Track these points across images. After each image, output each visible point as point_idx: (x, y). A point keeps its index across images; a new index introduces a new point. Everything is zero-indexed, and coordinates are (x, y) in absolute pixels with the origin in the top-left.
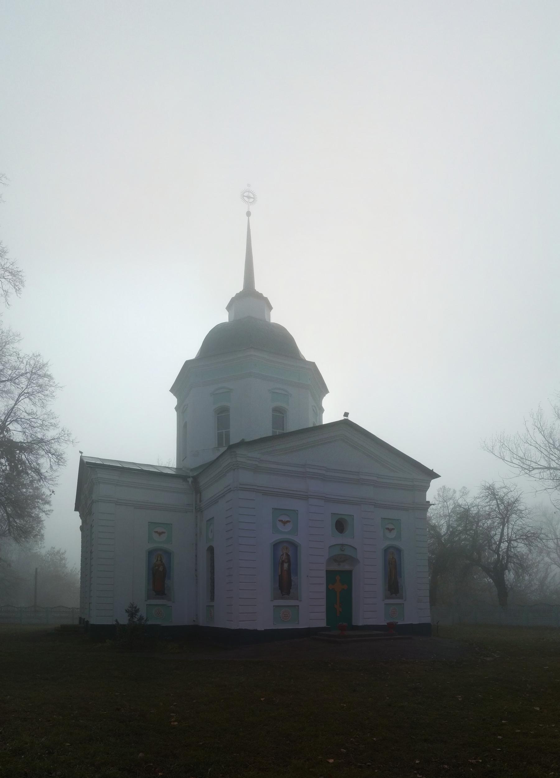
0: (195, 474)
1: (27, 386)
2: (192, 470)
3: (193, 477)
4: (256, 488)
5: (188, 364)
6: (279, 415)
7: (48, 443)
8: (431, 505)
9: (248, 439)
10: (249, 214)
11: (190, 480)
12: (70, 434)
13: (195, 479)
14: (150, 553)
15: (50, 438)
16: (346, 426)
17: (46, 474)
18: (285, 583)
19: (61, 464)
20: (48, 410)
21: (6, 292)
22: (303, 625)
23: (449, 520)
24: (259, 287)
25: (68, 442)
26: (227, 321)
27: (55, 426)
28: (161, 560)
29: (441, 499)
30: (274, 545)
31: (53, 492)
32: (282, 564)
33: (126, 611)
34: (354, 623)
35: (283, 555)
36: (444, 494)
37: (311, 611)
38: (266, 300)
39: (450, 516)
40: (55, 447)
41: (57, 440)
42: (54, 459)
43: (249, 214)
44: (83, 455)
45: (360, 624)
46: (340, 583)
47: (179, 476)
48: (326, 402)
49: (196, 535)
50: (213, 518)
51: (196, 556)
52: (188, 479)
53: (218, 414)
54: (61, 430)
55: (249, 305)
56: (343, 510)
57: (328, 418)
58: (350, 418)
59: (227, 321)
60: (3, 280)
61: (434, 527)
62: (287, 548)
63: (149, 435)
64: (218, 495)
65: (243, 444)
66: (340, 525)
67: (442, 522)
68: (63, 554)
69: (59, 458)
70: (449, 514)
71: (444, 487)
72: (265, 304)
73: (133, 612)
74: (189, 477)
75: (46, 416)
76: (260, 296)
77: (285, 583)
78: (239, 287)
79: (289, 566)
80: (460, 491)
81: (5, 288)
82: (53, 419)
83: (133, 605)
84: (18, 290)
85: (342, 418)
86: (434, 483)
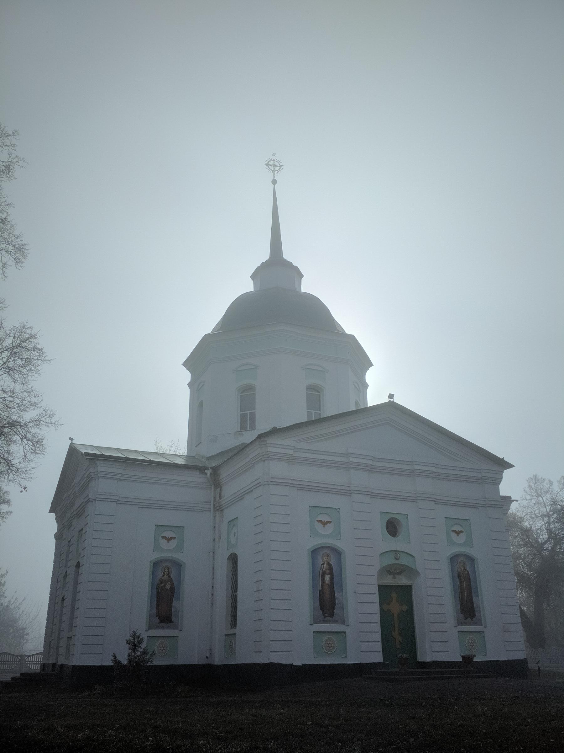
0: (214, 465)
1: (8, 359)
2: (209, 458)
3: (212, 468)
4: (290, 481)
5: (206, 336)
6: (314, 394)
7: (25, 425)
8: (513, 501)
10: (274, 182)
11: (209, 472)
12: (54, 414)
13: (215, 470)
14: (155, 564)
16: (391, 407)
17: (19, 466)
18: (327, 604)
19: (39, 452)
20: (30, 386)
21: (4, 264)
22: (351, 660)
23: (549, 523)
24: (288, 255)
25: (50, 425)
26: (252, 289)
28: (168, 575)
29: (533, 493)
30: (312, 552)
32: (323, 576)
33: (127, 641)
34: (420, 659)
35: (323, 564)
36: (536, 485)
37: (362, 642)
38: (296, 268)
39: (548, 516)
40: (33, 432)
41: (37, 422)
43: (274, 182)
44: (74, 442)
45: (428, 660)
46: (397, 602)
47: (191, 466)
48: (371, 376)
49: (214, 540)
50: (237, 518)
51: (213, 568)
52: (206, 471)
53: (242, 393)
54: (42, 410)
55: (277, 273)
56: (395, 508)
57: (374, 397)
58: (396, 400)
59: (252, 289)
60: (3, 253)
61: (527, 532)
63: (158, 419)
66: (392, 527)
67: (539, 524)
69: (37, 445)
70: (548, 513)
71: (535, 476)
72: (296, 274)
73: (134, 643)
74: (207, 468)
75: (25, 394)
76: (289, 265)
77: (327, 604)
78: (264, 255)
80: (559, 482)
81: (4, 260)
82: (35, 397)
83: (135, 634)
84: (18, 261)
85: (387, 400)
86: (507, 473)
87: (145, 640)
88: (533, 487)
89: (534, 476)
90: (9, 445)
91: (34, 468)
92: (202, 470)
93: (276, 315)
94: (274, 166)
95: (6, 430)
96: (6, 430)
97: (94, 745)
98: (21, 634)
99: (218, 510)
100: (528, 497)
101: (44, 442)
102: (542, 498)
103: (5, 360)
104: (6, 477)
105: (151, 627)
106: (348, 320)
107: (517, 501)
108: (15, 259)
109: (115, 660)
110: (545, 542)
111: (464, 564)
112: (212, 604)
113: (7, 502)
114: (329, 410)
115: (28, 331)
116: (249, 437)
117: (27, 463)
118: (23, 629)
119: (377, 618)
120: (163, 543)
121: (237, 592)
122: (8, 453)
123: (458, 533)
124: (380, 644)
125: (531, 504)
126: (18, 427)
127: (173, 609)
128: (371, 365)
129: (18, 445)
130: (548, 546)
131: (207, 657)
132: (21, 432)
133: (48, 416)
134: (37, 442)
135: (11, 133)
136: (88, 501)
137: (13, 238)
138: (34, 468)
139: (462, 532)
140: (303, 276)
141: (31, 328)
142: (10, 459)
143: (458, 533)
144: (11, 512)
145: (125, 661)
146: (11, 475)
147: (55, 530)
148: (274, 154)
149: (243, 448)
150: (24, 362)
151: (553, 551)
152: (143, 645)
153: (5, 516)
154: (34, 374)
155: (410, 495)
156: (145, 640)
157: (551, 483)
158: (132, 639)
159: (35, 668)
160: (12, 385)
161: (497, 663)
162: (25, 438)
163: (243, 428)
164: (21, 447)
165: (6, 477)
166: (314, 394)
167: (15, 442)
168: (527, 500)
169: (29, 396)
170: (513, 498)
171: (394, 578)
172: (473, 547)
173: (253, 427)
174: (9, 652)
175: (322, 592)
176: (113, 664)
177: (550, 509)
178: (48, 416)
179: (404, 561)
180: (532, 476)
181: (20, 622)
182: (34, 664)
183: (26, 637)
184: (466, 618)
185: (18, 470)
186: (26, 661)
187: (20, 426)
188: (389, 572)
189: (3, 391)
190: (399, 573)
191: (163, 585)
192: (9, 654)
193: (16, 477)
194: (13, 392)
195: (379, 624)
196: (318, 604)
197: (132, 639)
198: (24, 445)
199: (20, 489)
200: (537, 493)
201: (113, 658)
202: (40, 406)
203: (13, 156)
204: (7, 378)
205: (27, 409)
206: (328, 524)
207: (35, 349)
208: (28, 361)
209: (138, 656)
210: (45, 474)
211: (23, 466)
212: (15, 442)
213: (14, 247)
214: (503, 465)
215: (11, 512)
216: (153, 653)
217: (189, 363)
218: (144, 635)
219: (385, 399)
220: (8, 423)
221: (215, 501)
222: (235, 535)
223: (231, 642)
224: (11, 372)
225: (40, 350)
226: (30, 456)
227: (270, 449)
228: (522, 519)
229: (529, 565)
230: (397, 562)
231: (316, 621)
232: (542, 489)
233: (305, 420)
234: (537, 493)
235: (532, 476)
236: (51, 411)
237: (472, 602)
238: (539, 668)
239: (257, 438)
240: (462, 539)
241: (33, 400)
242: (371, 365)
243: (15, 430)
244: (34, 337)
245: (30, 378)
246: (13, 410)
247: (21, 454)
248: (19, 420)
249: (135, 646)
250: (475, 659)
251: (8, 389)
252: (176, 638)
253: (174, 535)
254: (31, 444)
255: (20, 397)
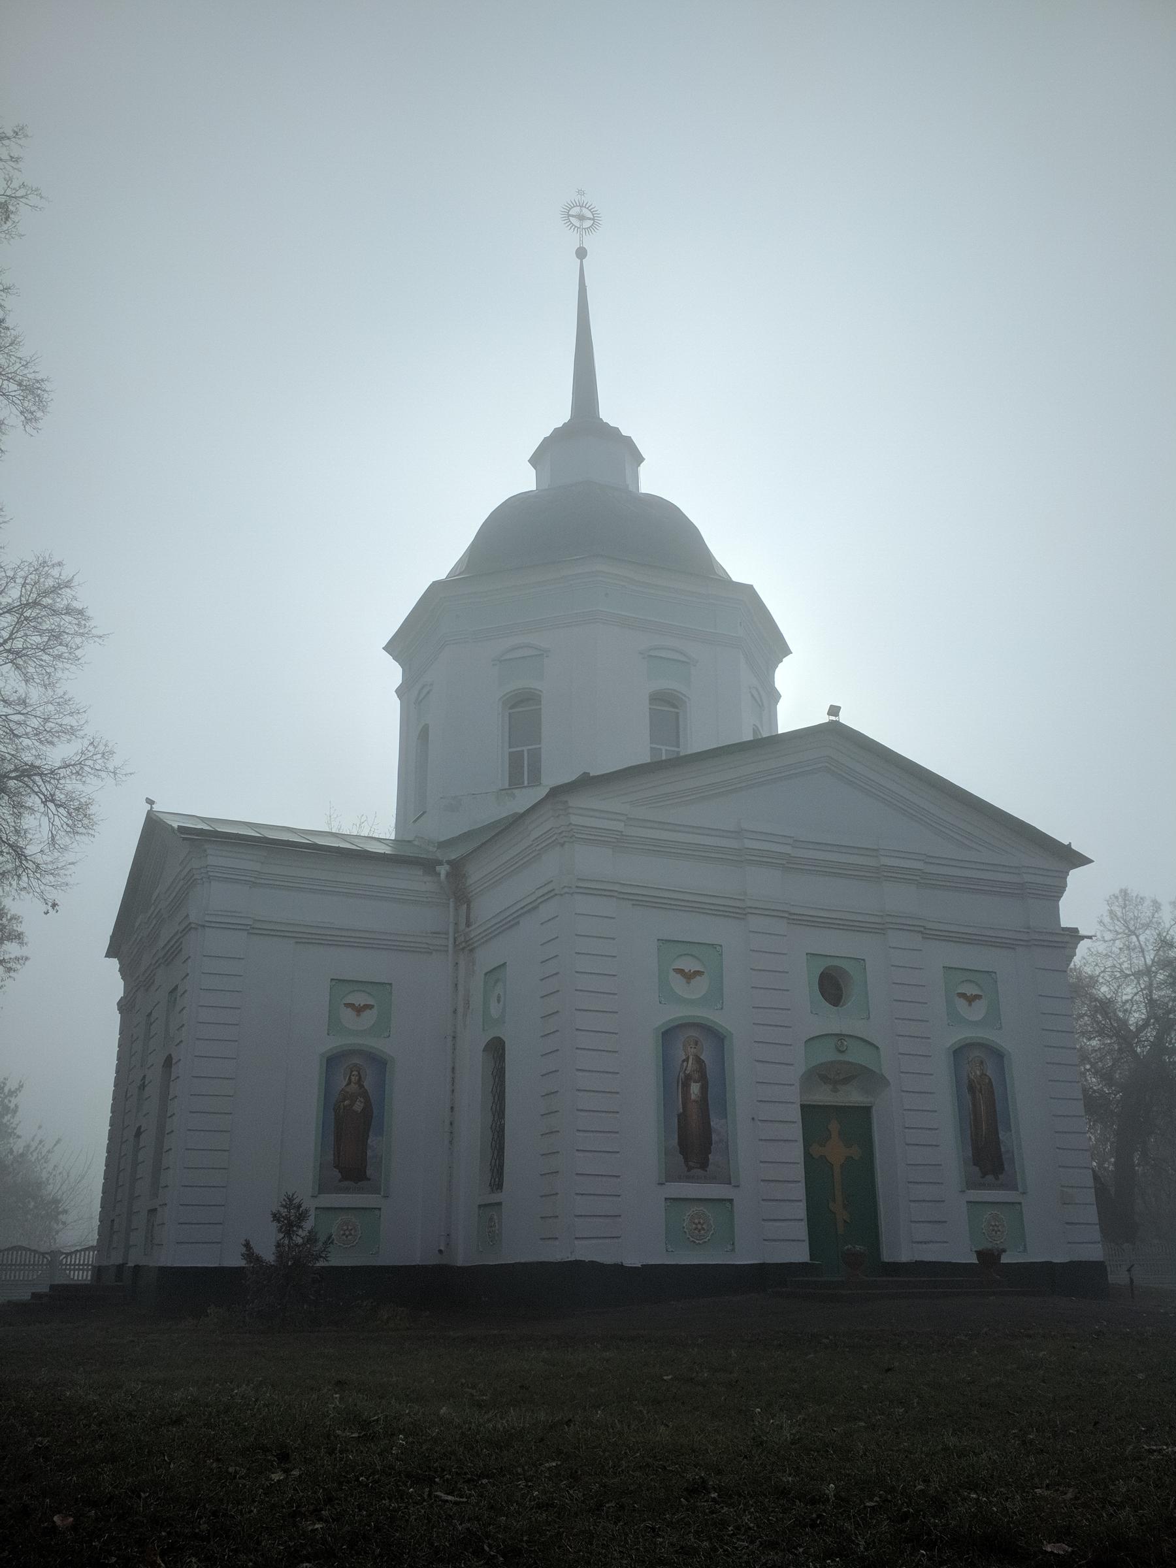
2: (442, 845)
3: (449, 862)
5: (436, 586)
6: (667, 709)
8: (1083, 938)
9: (593, 773)
10: (581, 253)
11: (443, 870)
12: (112, 753)
13: (457, 869)
15: (58, 765)
16: (835, 741)
17: (39, 859)
18: (694, 1142)
19: (82, 830)
20: (60, 692)
22: (745, 1256)
23: (1150, 986)
24: (610, 412)
25: (103, 774)
27: (72, 731)
28: (360, 1083)
29: (1119, 927)
31: (54, 905)
33: (274, 1215)
34: (887, 1257)
35: (687, 1060)
37: (768, 1222)
38: (628, 443)
39: (1147, 971)
40: (69, 788)
41: (76, 768)
42: (60, 818)
43: (581, 253)
44: (156, 808)
45: (904, 1258)
46: (840, 1139)
47: (401, 858)
48: (785, 676)
49: (455, 1011)
52: (438, 868)
54: (86, 743)
55: (587, 450)
56: (838, 946)
57: (792, 715)
58: (844, 718)
61: (1105, 1007)
62: (696, 1043)
63: (332, 761)
64: (529, 900)
65: (586, 782)
66: (832, 986)
67: (1128, 992)
68: (12, 1093)
69: (78, 815)
71: (1125, 893)
73: (289, 1219)
74: (440, 863)
75: (51, 708)
76: (613, 434)
77: (694, 1142)
78: (562, 414)
79: (704, 1089)
82: (71, 714)
84: (29, 418)
85: (825, 719)
86: (1075, 877)
87: (312, 1213)
88: (1119, 914)
89: (1121, 891)
90: (19, 816)
91: (73, 863)
92: (428, 866)
93: (586, 544)
94: (581, 218)
95: (12, 783)
96: (12, 783)
97: (210, 1413)
98: (52, 1210)
99: (463, 948)
100: (1108, 936)
101: (92, 810)
102: (1137, 937)
103: (6, 635)
104: (14, 883)
105: (323, 1187)
106: (737, 557)
107: (1090, 937)
108: (22, 413)
109: (249, 1254)
110: (1140, 1029)
111: (982, 1063)
112: (451, 1142)
113: (18, 937)
114: (698, 739)
115: (55, 572)
116: (524, 799)
117: (56, 854)
118: (56, 1201)
119: (799, 1172)
120: (348, 1016)
121: (503, 1117)
122: (17, 832)
123: (971, 999)
124: (803, 1226)
125: (1114, 949)
126: (37, 778)
127: (369, 1153)
128: (786, 651)
129: (38, 815)
130: (1150, 1034)
131: (440, 1251)
132: (44, 790)
133: (99, 756)
134: (77, 809)
135: (10, 134)
136: (188, 929)
137: (18, 365)
138: (73, 863)
139: (978, 997)
140: (642, 459)
141: (60, 564)
142: (21, 843)
143: (971, 999)
144: (27, 959)
145: (268, 1255)
146: (25, 878)
147: (120, 993)
148: (581, 192)
149: (516, 821)
150: (46, 639)
151: (1159, 1046)
152: (308, 1224)
153: (14, 966)
154: (68, 666)
155: (873, 919)
156: (312, 1213)
157: (1157, 906)
158: (284, 1212)
159: (83, 1276)
160: (22, 689)
161: (1048, 1268)
162: (53, 801)
163: (515, 781)
164: (45, 820)
165: (14, 883)
166: (667, 709)
167: (31, 810)
168: (1105, 941)
169: (59, 712)
170: (1082, 932)
171: (835, 1090)
172: (1000, 1028)
173: (535, 779)
174: (25, 1244)
175: (683, 1118)
176: (242, 1263)
177: (1153, 961)
178: (99, 756)
179: (857, 1056)
180: (1117, 892)
181: (50, 1187)
182: (79, 1270)
183: (62, 1217)
184: (984, 1175)
185: (38, 866)
186: (61, 1264)
187: (41, 775)
188: (825, 1079)
189: (4, 701)
190: (846, 1081)
191: (347, 1103)
192: (25, 1249)
193: (34, 882)
194: (23, 702)
195: (802, 1185)
196: (674, 1141)
197: (284, 1212)
198: (51, 815)
199: (44, 908)
200: (1128, 927)
201: (244, 1250)
202: (81, 733)
203: (15, 184)
204: (12, 673)
205: (55, 740)
206: (698, 978)
207: (69, 611)
208: (56, 636)
209: (297, 1245)
210: (96, 874)
211: (49, 859)
212: (31, 810)
213: (20, 384)
214: (1072, 858)
215: (27, 959)
216: (329, 1240)
217: (398, 647)
218: (309, 1204)
219: (821, 717)
220: (16, 770)
221: (456, 931)
222: (499, 1001)
223: (491, 1219)
224: (20, 661)
225: (81, 612)
226: (63, 839)
227: (574, 819)
228: (1093, 981)
229: (1106, 1077)
230: (841, 1057)
231: (670, 1176)
232: (1136, 918)
233: (647, 759)
234: (1128, 927)
235: (1117, 892)
236: (106, 745)
237: (998, 1142)
238: (1132, 1281)
239: (547, 796)
240: (977, 1012)
241: (67, 720)
242: (786, 651)
243: (31, 784)
244: (68, 584)
245: (59, 674)
246: (26, 742)
247: (45, 833)
248: (38, 763)
249: (291, 1224)
250: (1004, 1259)
251: (14, 697)
252: (377, 1212)
253: (370, 1002)
254: (65, 814)
255: (38, 714)
